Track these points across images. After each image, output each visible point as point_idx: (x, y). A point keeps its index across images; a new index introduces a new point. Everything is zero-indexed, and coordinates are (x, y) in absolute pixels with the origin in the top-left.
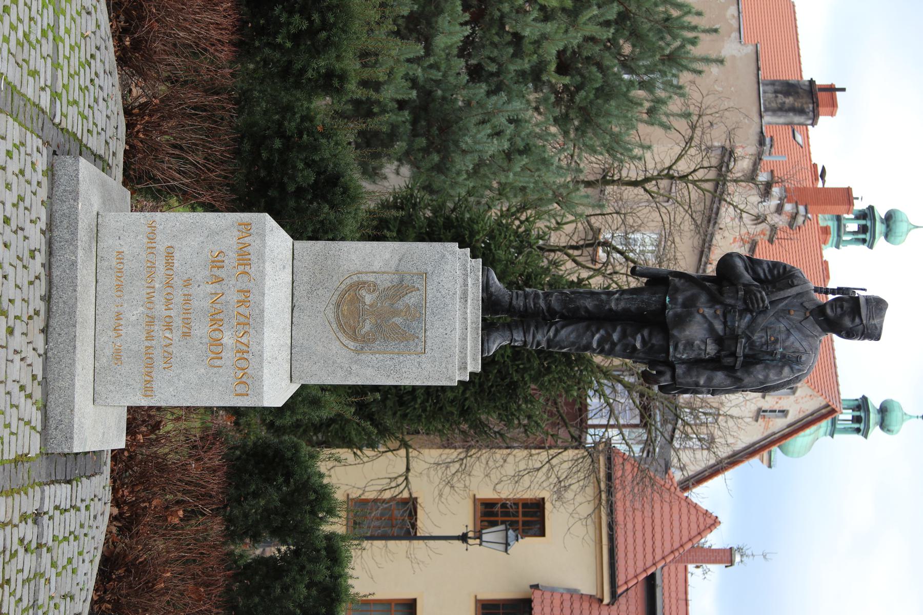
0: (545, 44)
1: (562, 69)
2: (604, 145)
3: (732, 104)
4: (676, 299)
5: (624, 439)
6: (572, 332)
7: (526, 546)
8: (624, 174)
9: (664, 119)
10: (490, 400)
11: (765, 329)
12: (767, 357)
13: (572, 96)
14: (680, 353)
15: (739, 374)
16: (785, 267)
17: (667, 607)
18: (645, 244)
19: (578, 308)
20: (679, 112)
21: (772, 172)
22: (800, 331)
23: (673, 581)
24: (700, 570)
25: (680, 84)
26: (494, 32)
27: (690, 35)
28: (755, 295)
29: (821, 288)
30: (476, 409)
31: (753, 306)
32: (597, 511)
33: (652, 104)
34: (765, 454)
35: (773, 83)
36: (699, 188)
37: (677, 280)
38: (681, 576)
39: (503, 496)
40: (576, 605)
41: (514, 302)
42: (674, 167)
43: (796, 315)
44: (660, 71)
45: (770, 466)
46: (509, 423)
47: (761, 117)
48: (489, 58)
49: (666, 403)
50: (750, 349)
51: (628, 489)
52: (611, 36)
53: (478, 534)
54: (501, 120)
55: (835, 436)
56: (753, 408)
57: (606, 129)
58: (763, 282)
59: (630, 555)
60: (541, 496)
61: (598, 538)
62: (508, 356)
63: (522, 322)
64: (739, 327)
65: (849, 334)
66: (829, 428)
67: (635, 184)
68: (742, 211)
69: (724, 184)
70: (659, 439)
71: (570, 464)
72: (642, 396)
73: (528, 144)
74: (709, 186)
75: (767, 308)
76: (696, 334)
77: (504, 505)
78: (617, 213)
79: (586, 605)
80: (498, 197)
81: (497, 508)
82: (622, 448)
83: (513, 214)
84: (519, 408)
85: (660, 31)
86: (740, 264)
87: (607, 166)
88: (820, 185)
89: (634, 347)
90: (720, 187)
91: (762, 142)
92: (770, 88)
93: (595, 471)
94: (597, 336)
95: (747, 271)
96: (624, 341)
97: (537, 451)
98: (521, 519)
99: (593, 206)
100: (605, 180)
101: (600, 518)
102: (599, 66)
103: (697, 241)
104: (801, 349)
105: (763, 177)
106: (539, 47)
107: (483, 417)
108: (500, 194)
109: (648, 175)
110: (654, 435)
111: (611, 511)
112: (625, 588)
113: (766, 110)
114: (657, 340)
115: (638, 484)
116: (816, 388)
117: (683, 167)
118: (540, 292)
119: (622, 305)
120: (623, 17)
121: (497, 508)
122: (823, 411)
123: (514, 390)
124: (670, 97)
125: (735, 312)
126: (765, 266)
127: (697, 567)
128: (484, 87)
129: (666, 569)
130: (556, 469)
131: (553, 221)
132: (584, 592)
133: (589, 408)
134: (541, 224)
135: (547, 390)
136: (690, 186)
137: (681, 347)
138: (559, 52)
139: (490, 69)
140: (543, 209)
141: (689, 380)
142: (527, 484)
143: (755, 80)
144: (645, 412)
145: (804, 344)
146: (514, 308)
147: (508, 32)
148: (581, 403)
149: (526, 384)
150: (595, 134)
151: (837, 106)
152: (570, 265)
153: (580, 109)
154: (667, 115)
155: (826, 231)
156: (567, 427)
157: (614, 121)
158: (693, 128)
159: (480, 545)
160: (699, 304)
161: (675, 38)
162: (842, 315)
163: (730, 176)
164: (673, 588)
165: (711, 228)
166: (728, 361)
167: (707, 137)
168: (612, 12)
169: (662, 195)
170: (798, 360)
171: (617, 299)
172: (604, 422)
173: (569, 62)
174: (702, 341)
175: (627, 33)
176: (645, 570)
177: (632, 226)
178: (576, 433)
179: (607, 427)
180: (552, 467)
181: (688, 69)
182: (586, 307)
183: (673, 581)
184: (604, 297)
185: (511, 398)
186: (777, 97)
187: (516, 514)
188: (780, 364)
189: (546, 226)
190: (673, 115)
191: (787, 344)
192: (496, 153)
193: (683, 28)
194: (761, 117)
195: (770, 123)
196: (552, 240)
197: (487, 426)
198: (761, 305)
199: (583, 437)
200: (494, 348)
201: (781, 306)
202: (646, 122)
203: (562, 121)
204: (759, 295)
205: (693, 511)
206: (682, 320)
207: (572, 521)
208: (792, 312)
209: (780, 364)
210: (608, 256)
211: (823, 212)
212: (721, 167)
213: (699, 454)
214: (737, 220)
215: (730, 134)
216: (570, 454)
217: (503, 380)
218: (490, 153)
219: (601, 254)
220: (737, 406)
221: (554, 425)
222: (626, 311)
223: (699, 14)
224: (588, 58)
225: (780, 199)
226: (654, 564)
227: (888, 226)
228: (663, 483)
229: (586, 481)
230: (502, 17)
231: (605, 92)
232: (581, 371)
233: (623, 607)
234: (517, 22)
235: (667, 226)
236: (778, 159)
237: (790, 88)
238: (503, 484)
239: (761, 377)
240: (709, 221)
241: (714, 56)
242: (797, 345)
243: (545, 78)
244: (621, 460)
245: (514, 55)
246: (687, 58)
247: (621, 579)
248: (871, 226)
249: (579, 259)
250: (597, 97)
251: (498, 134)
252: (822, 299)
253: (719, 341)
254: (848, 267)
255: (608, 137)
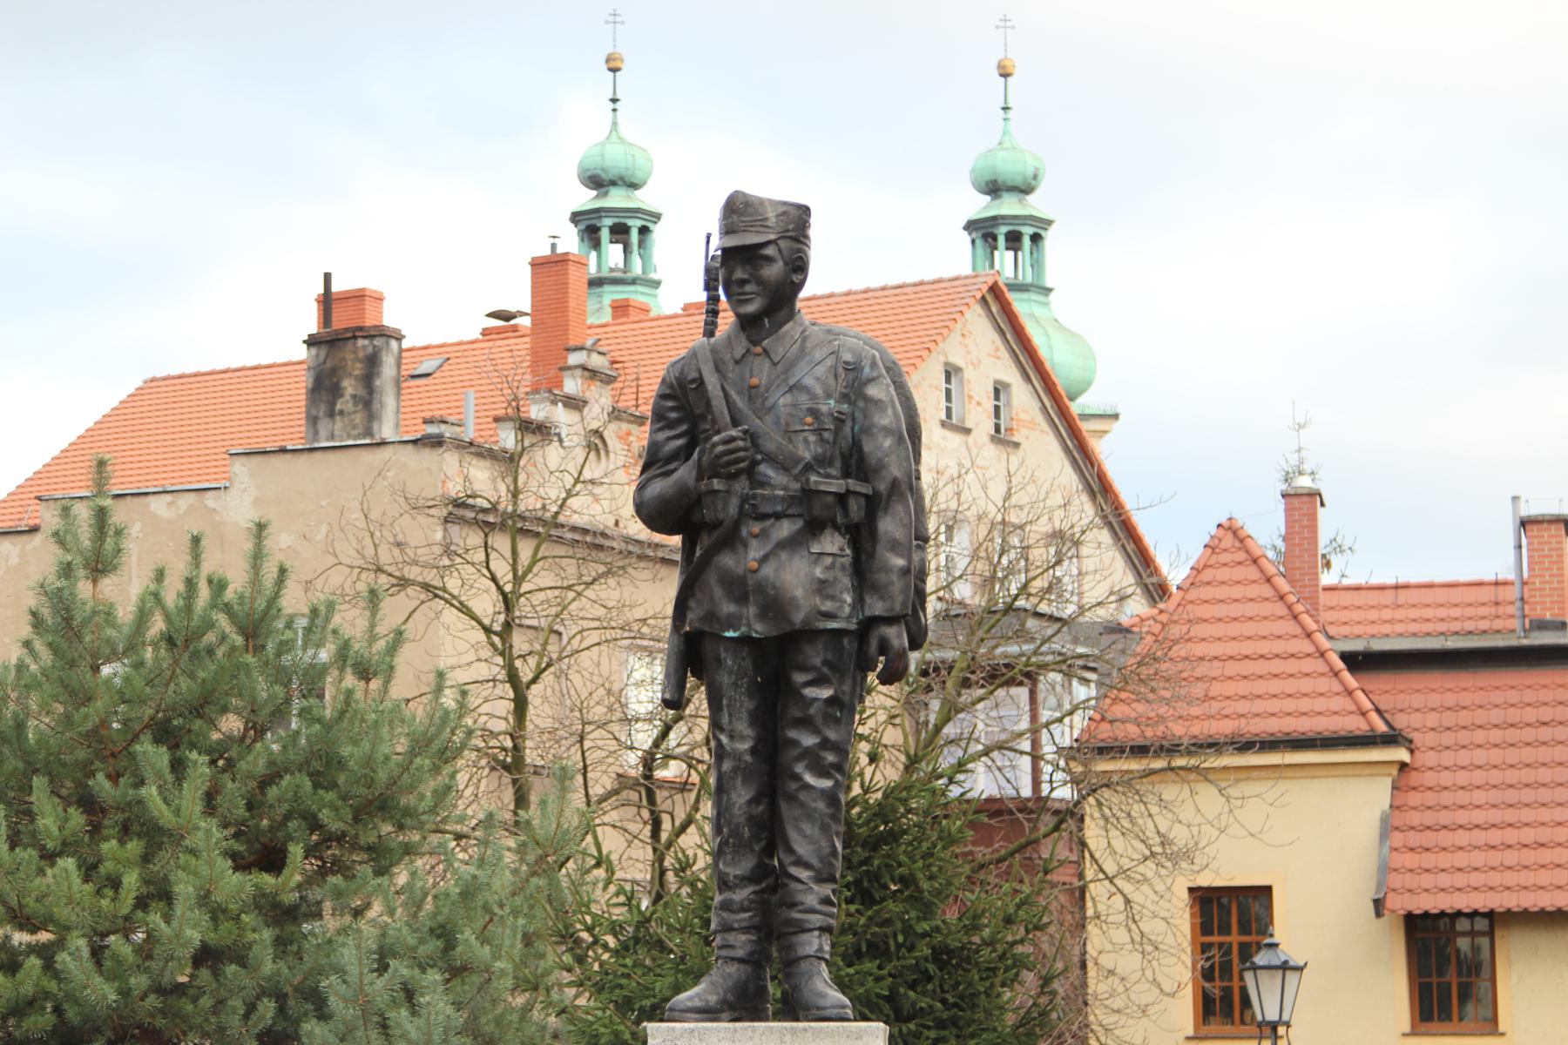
0: (218, 897)
1: (272, 860)
2: (436, 770)
3: (356, 505)
4: (729, 616)
5: (1060, 720)
6: (800, 831)
7: (1291, 930)
8: (500, 726)
9: (380, 645)
10: (974, 1006)
11: (789, 434)
12: (847, 429)
13: (329, 838)
14: (841, 607)
15: (882, 487)
16: (662, 397)
17: (1414, 628)
18: (644, 681)
19: (751, 819)
20: (367, 613)
21: (497, 420)
22: (792, 365)
23: (1357, 615)
24: (1333, 559)
25: (306, 610)
26: (190, 1008)
27: (204, 593)
28: (718, 457)
29: (706, 323)
30: (992, 1035)
31: (743, 460)
32: (1211, 776)
33: (349, 670)
34: (1085, 427)
35: (313, 421)
36: (529, 569)
37: (690, 616)
38: (1346, 599)
39: (1187, 976)
40: (1415, 818)
41: (740, 953)
42: (487, 622)
43: (761, 373)
44: (279, 655)
45: (1116, 416)
46: (1020, 963)
47: (383, 443)
48: (246, 1016)
49: (980, 633)
50: (831, 464)
51: (1163, 710)
52: (205, 759)
53: (1267, 1031)
54: (379, 988)
55: (1048, 285)
56: (990, 454)
57: (399, 765)
58: (694, 440)
59: (1304, 705)
60: (1185, 895)
61: (1269, 773)
62: (880, 968)
63: (781, 936)
64: (785, 488)
65: (798, 266)
66: (1034, 296)
67: (520, 705)
68: (577, 481)
69: (523, 518)
70: (1056, 647)
71: (1114, 833)
72: (966, 683)
73: (432, 931)
74: (526, 549)
75: (745, 432)
76: (806, 575)
77: (1208, 975)
78: (581, 741)
79: (1414, 798)
80: (542, 991)
81: (1215, 989)
82: (1079, 721)
83: (581, 960)
84: (990, 943)
85: (195, 655)
86: (658, 487)
87: (483, 762)
88: (525, 322)
89: (831, 701)
90: (528, 526)
91: (436, 442)
92: (324, 427)
93: (1127, 781)
94: (809, 779)
95: (672, 472)
96: (819, 721)
97: (1089, 904)
98: (1235, 938)
99: (564, 790)
100: (513, 765)
101: (1226, 768)
102: (266, 782)
103: (642, 572)
104: (829, 362)
105: (508, 438)
106: (224, 911)
107: (1010, 1019)
108: (536, 989)
109: (502, 675)
110: (1050, 658)
111: (1211, 745)
112: (1374, 716)
113: (368, 432)
114: (816, 655)
115: (1153, 690)
116: (948, 322)
117: (486, 604)
118: (718, 898)
119: (743, 727)
120: (164, 733)
121: (1215, 989)
122: (994, 309)
123: (950, 952)
124: (335, 632)
125: (754, 497)
126: (661, 436)
127: (1328, 565)
128: (310, 1026)
129: (1332, 630)
130: (1126, 864)
131: (596, 872)
132: (1385, 802)
133: (995, 793)
134: (603, 900)
135: (949, 883)
136: (525, 587)
137: (828, 606)
138: (237, 868)
139: (270, 1014)
140: (570, 898)
141: (897, 585)
142: (1160, 926)
143: (305, 457)
144: (1000, 676)
145: (818, 355)
146: (751, 954)
147: (191, 976)
148: (977, 812)
149: (937, 929)
150: (411, 788)
151: (363, 290)
152: (690, 840)
153: (356, 820)
154: (372, 637)
155: (620, 309)
156: (1036, 841)
157: (385, 749)
158: (403, 583)
159: (1288, 1025)
160: (740, 570)
161: (210, 625)
162: (760, 281)
163: (506, 505)
164: (1372, 615)
165: (615, 544)
166: (856, 509)
167: (424, 555)
168: (153, 755)
169: (545, 644)
170: (853, 369)
171: (732, 737)
172: (1026, 762)
173: (257, 846)
174: (816, 562)
175: (197, 724)
176: (1336, 674)
177: (611, 709)
178: (1048, 821)
179: (1036, 758)
180: (1123, 872)
181: (277, 595)
182: (750, 802)
183: (1357, 615)
184: (727, 766)
185: (968, 961)
186: (341, 413)
187: (1226, 950)
188: (861, 404)
189: (605, 888)
190: (372, 626)
191: (819, 391)
192: (451, 997)
193: (188, 608)
194: (383, 443)
195: (397, 425)
196: (639, 876)
197: (1028, 1012)
198: (741, 443)
199: (1057, 806)
200: (836, 996)
201: (740, 403)
202: (387, 682)
203: (382, 859)
204: (721, 448)
205: (1207, 575)
206: (774, 605)
207: (1235, 829)
208: (755, 381)
209: (861, 404)
210: (675, 758)
211: (583, 313)
212: (486, 523)
213: (1089, 565)
214: (597, 490)
215: (417, 508)
216: (1093, 833)
217: (930, 979)
218: (449, 1010)
219: (672, 771)
220: (984, 488)
221: (1029, 865)
222: (756, 719)
223: (160, 575)
224: (250, 806)
225: (554, 403)
226: (1322, 655)
227: (613, 183)
228: (1149, 639)
229: (1149, 798)
230: (159, 990)
231: (323, 767)
232: (909, 811)
233: (1416, 720)
234: (172, 958)
235: (609, 634)
236: (472, 408)
237: (324, 387)
238: (1160, 978)
239: (887, 443)
240: (600, 547)
241: (249, 546)
242: (820, 371)
243: (290, 898)
244: (1105, 726)
245: (242, 961)
246: (253, 599)
247: (1356, 725)
248: (612, 221)
249: (680, 817)
250: (333, 785)
251: (409, 994)
252: (727, 320)
253: (814, 527)
254: (678, 271)
255: (418, 760)
